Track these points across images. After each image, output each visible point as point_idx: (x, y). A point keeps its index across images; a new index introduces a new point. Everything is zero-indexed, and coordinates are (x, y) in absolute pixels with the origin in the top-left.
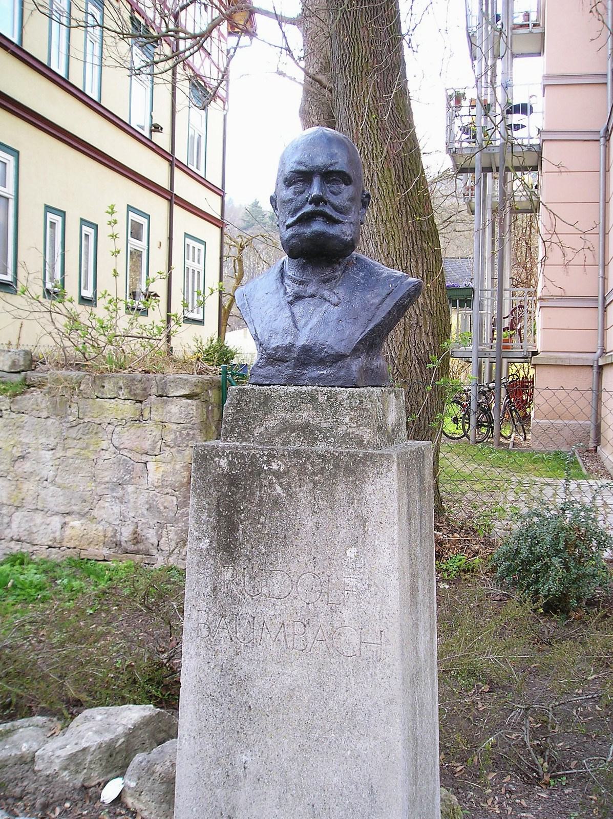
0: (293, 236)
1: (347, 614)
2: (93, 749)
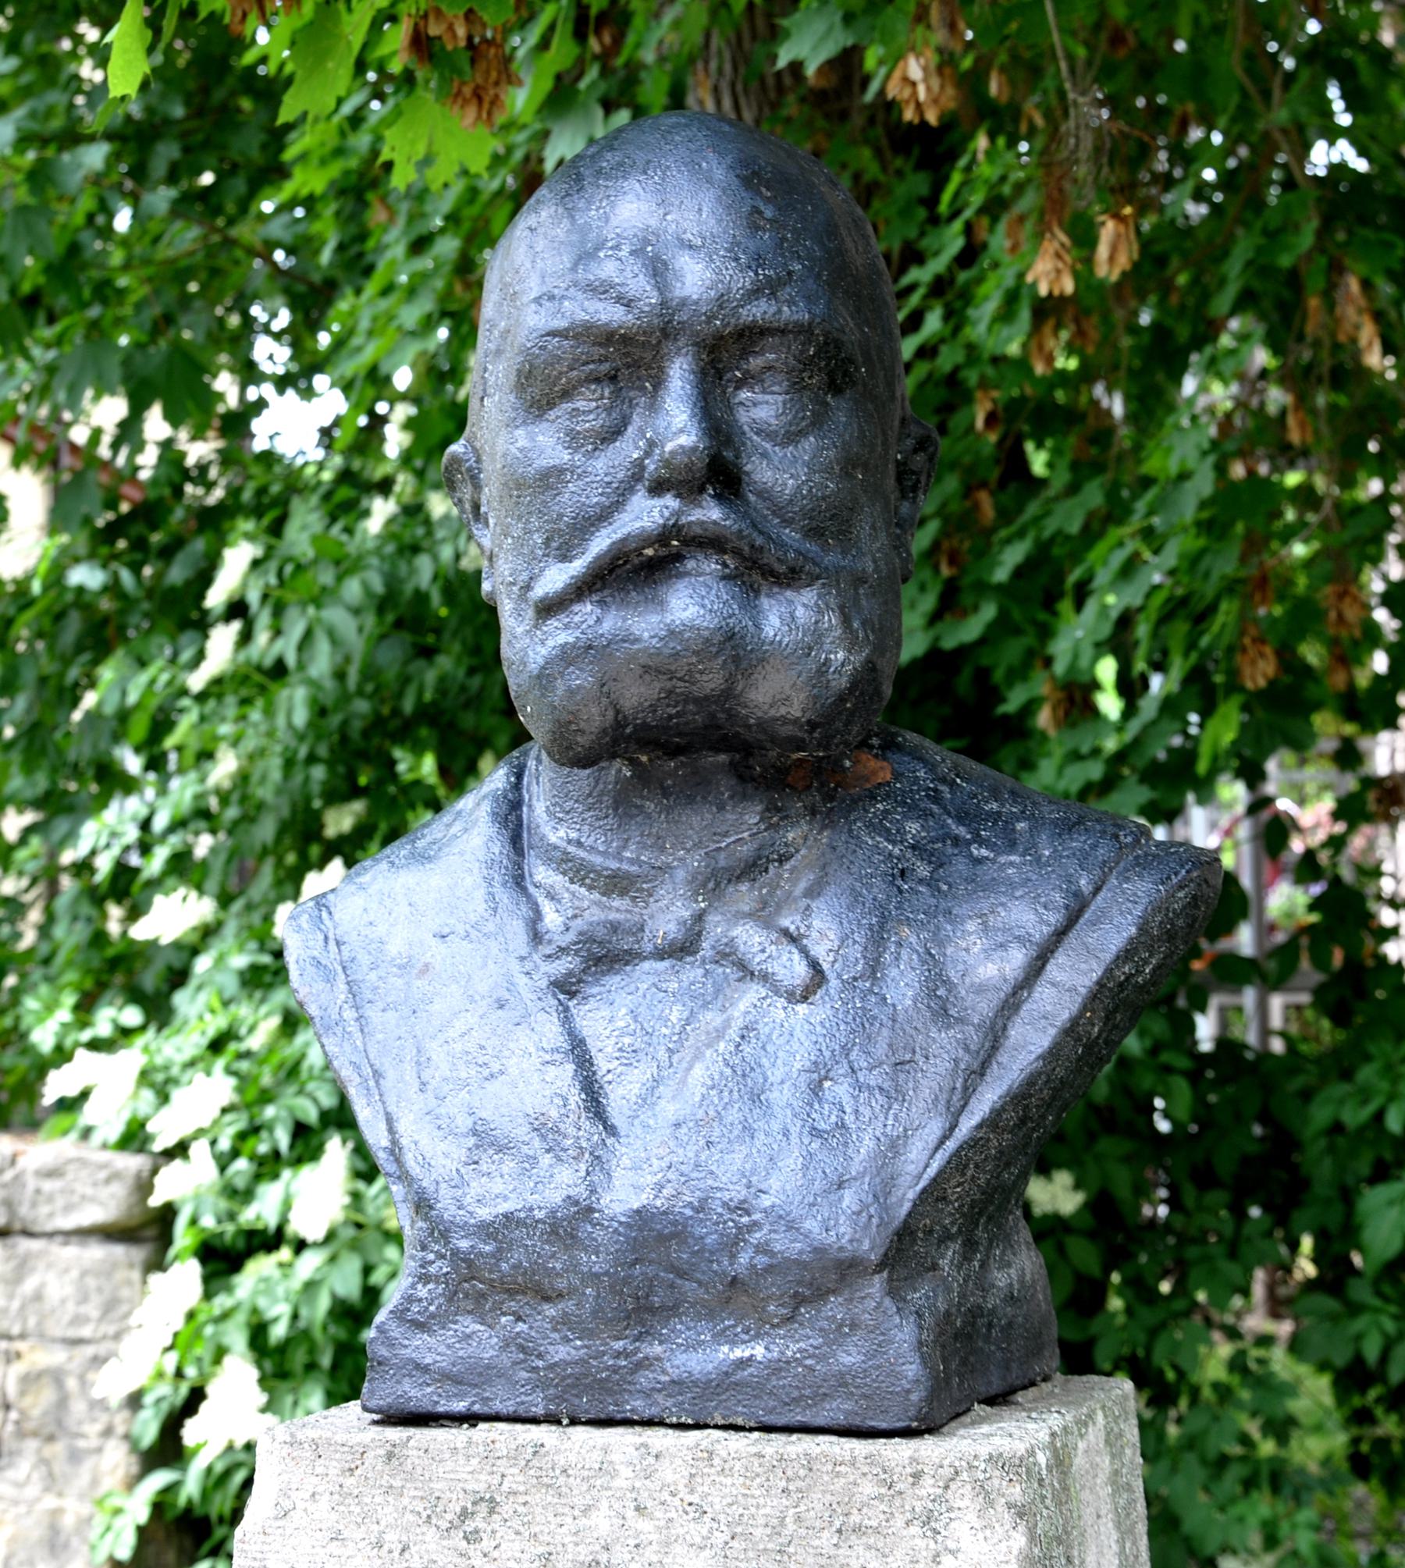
0: (567, 657)
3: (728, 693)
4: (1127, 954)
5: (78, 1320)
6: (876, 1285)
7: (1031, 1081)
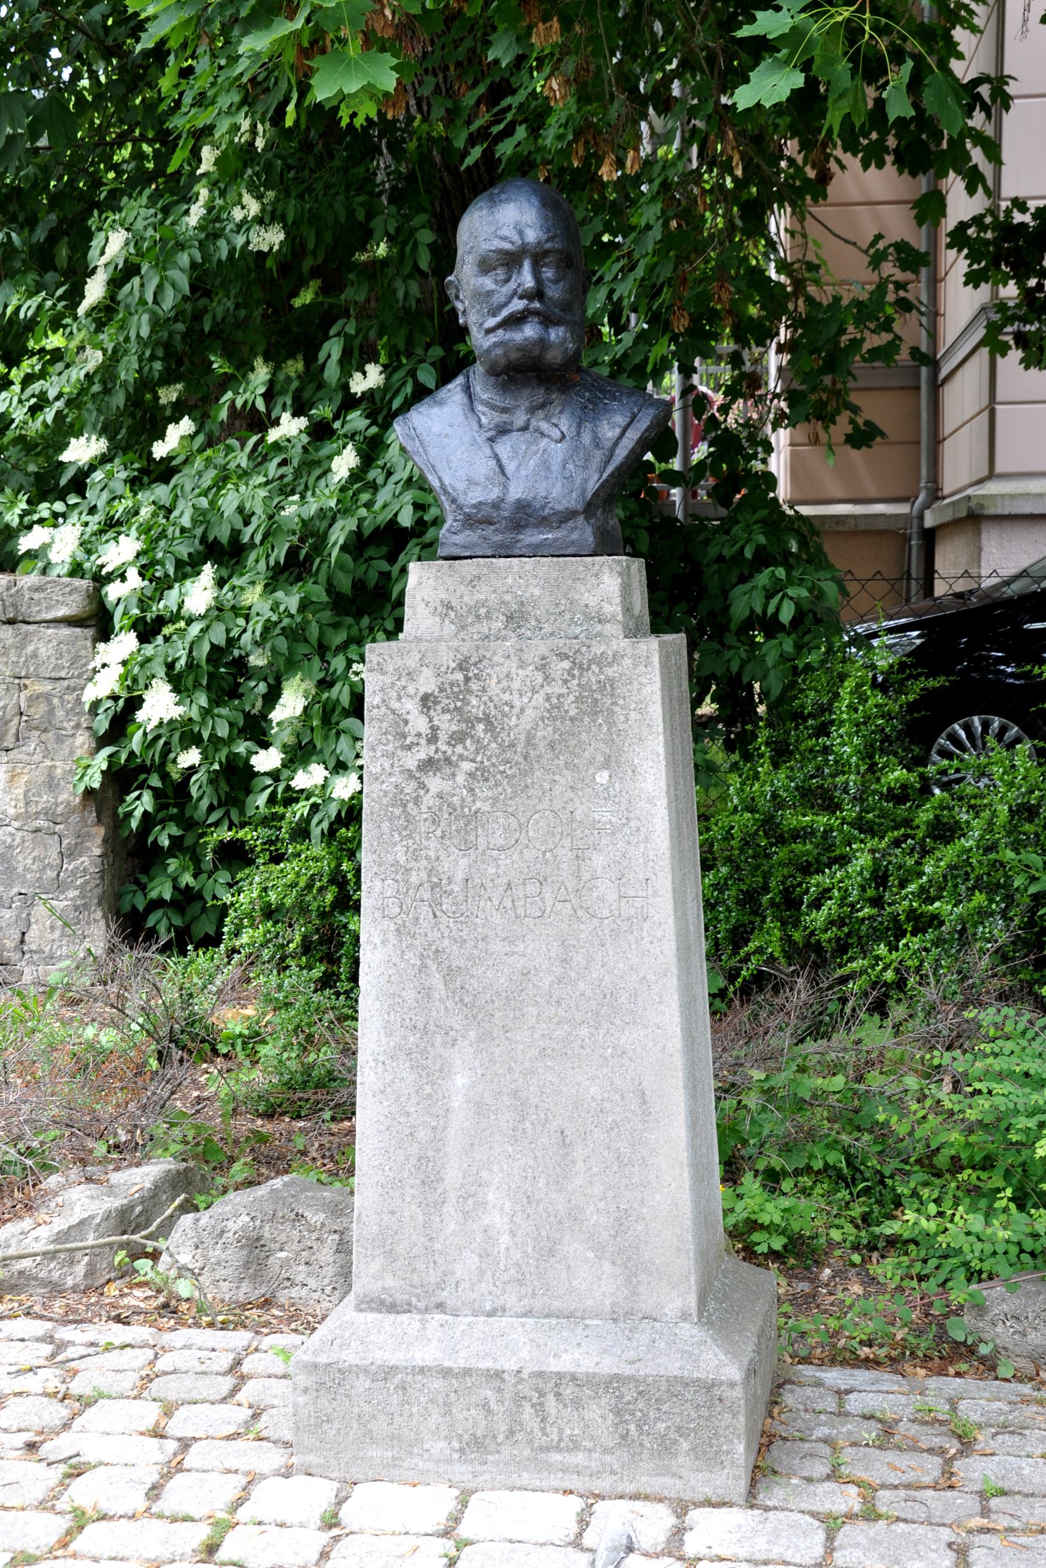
0: (496, 345)
1: (598, 860)
2: (97, 1220)
3: (540, 356)
4: (647, 430)
5: (56, 668)
6: (581, 518)
7: (622, 464)
